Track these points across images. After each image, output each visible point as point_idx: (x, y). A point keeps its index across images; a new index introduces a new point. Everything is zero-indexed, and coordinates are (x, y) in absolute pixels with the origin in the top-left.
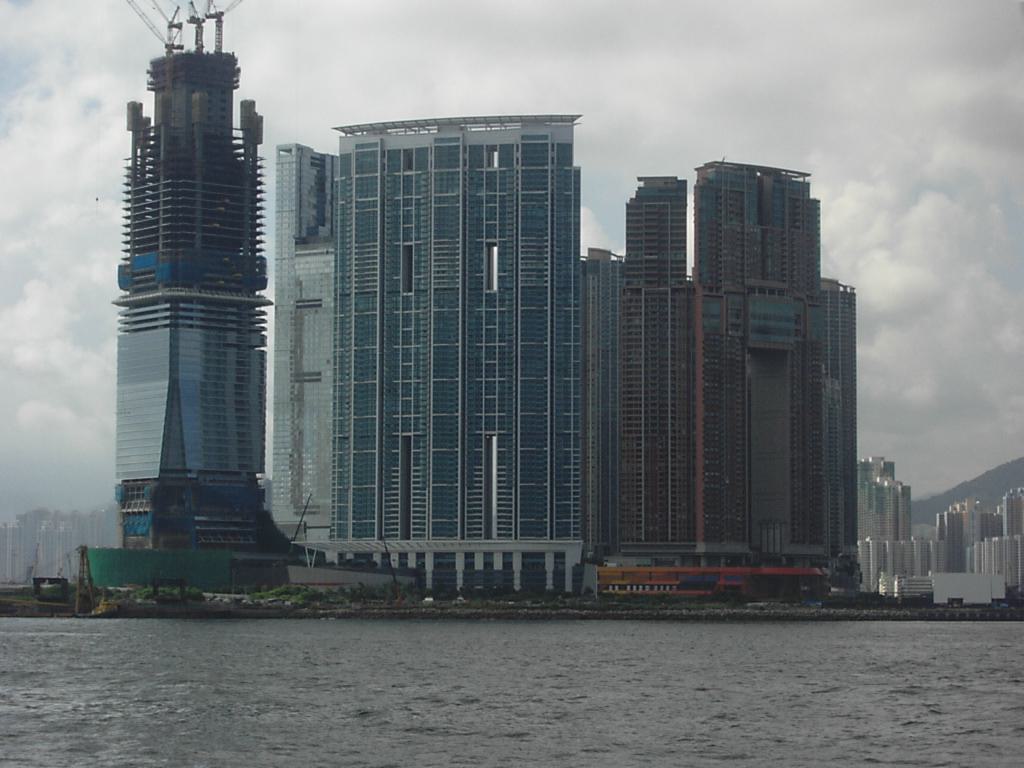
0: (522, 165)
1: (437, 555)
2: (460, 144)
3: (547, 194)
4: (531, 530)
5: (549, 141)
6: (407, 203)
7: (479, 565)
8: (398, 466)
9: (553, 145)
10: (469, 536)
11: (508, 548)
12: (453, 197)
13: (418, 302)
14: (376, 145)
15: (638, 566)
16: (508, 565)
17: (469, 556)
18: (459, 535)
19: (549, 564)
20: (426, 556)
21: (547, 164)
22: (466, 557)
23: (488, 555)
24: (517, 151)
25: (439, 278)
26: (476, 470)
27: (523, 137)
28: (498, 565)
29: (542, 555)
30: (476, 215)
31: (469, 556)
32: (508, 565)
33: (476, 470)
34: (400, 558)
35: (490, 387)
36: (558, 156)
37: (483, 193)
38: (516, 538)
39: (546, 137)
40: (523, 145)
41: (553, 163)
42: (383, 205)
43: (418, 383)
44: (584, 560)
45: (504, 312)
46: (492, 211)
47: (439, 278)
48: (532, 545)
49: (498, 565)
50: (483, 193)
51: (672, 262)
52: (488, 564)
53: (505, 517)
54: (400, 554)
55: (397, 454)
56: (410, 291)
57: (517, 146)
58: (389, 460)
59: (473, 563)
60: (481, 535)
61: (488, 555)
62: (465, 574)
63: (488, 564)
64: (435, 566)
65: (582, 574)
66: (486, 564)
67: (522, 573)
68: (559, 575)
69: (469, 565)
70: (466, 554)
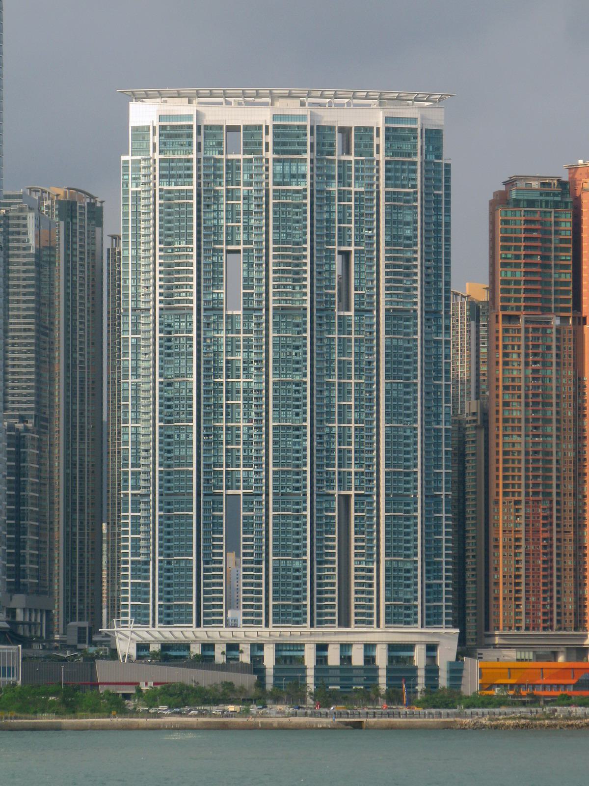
0: (161, 152)
1: (279, 647)
2: (194, 123)
3: (416, 193)
4: (283, 616)
5: (418, 126)
6: (343, 195)
7: (334, 658)
8: (221, 533)
9: (312, 128)
10: (206, 622)
11: (370, 638)
12: (298, 192)
13: (359, 325)
14: (190, 117)
15: (518, 660)
16: (369, 660)
17: (322, 648)
18: (151, 622)
19: (419, 658)
20: (265, 648)
21: (305, 152)
22: (389, 650)
23: (345, 647)
24: (154, 134)
25: (280, 293)
26: (214, 539)
27: (161, 118)
28: (358, 659)
29: (410, 647)
30: (325, 216)
31: (322, 648)
32: (369, 660)
33: (214, 539)
34: (252, 650)
35: (343, 436)
36: (372, 139)
37: (334, 188)
38: (378, 626)
39: (414, 120)
40: (275, 127)
41: (312, 151)
42: (199, 195)
43: (250, 428)
44: (460, 654)
45: (361, 340)
46: (343, 210)
47: (280, 293)
48: (400, 635)
49: (358, 659)
50: (334, 188)
51: (556, 283)
52: (346, 659)
53: (364, 599)
54: (252, 645)
55: (221, 517)
56: (348, 309)
57: (267, 127)
58: (321, 525)
59: (326, 658)
60: (333, 622)
61: (345, 647)
62: (316, 669)
63: (346, 659)
64: (277, 660)
65: (461, 671)
66: (253, 658)
67: (389, 670)
68: (432, 671)
69: (321, 660)
70: (277, 645)
